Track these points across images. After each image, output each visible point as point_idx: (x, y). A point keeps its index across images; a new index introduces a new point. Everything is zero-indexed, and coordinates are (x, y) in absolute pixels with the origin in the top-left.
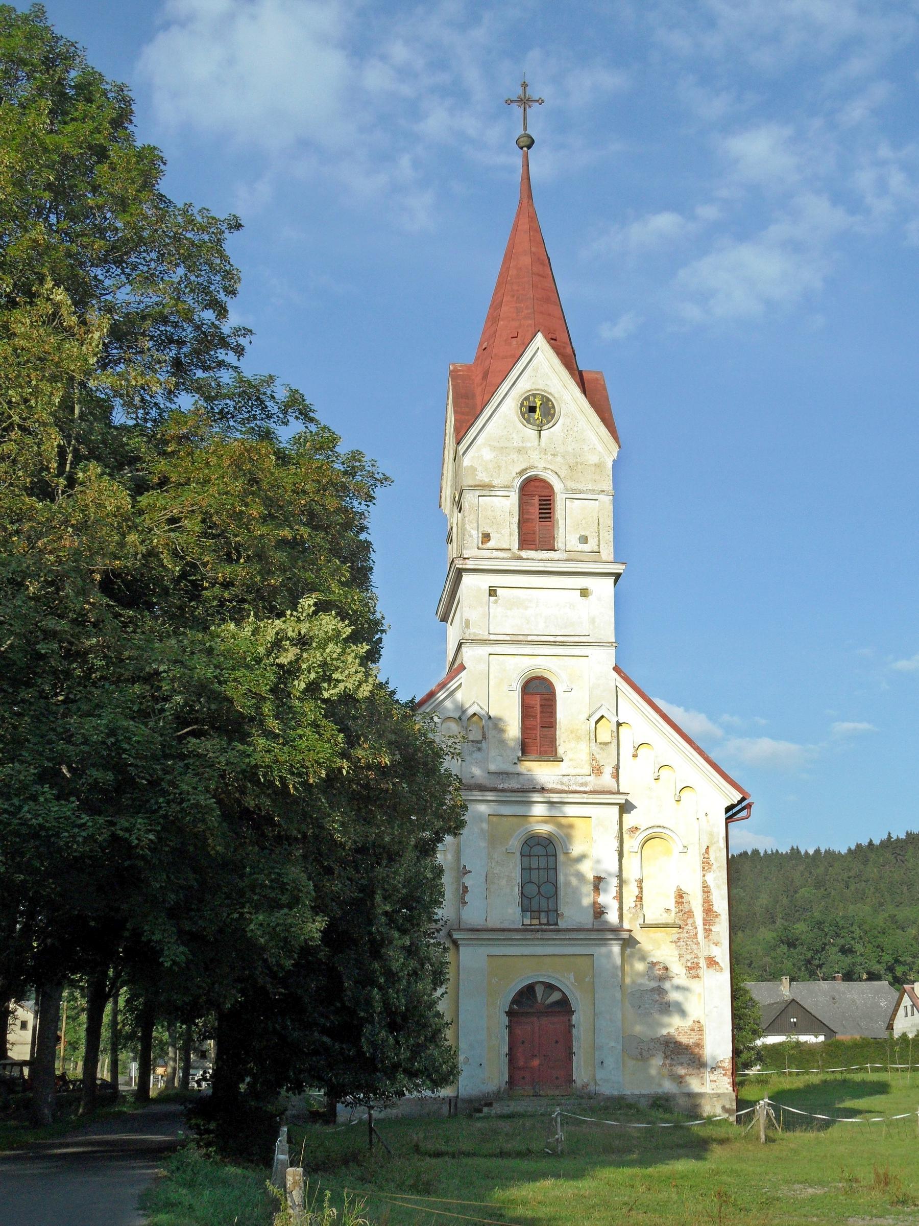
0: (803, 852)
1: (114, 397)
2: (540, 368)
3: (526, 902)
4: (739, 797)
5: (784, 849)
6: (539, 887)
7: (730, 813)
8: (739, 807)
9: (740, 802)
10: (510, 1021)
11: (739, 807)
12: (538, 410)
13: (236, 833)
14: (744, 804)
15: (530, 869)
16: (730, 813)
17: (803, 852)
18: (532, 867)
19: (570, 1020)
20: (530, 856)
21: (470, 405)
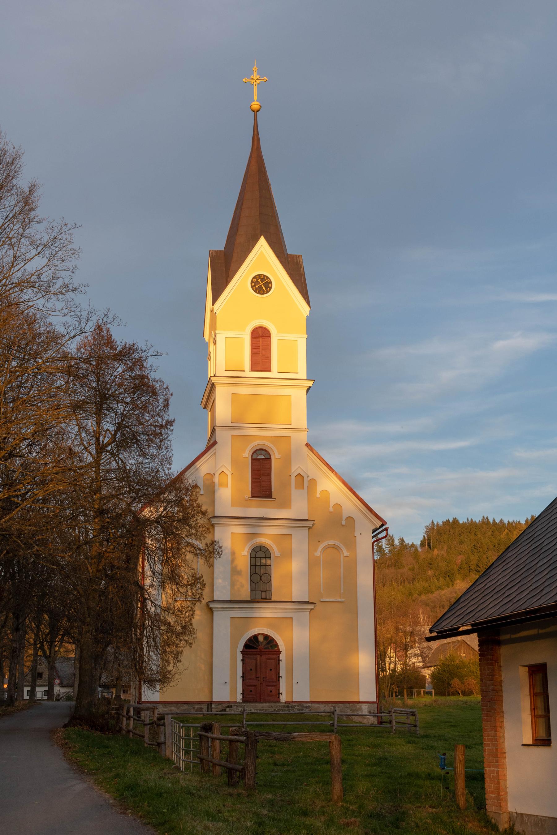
0: (491, 521)
1: (100, 493)
2: (262, 257)
3: (254, 585)
4: (380, 523)
5: (478, 519)
6: (261, 577)
7: (375, 533)
8: (381, 529)
9: (381, 527)
10: (243, 657)
11: (381, 529)
12: (262, 285)
13: (224, 821)
14: (384, 527)
15: (256, 565)
16: (375, 533)
17: (491, 521)
18: (257, 564)
19: (279, 657)
20: (255, 557)
21: (224, 267)
